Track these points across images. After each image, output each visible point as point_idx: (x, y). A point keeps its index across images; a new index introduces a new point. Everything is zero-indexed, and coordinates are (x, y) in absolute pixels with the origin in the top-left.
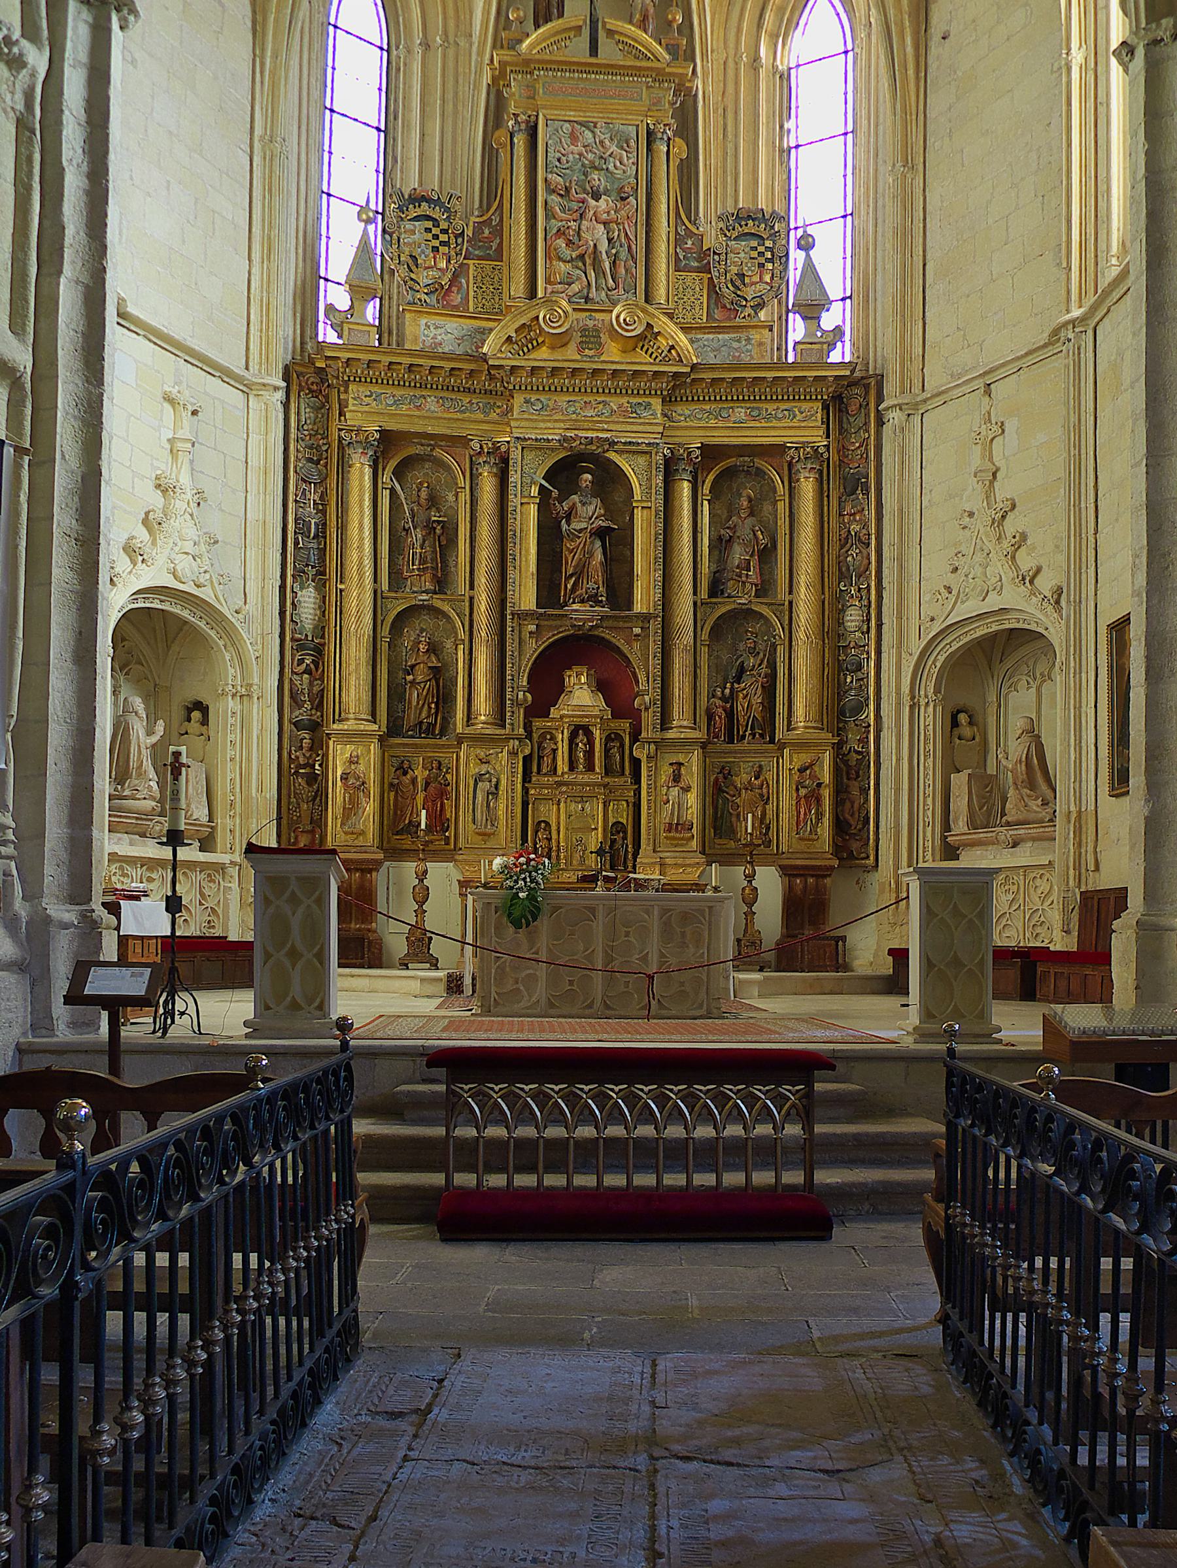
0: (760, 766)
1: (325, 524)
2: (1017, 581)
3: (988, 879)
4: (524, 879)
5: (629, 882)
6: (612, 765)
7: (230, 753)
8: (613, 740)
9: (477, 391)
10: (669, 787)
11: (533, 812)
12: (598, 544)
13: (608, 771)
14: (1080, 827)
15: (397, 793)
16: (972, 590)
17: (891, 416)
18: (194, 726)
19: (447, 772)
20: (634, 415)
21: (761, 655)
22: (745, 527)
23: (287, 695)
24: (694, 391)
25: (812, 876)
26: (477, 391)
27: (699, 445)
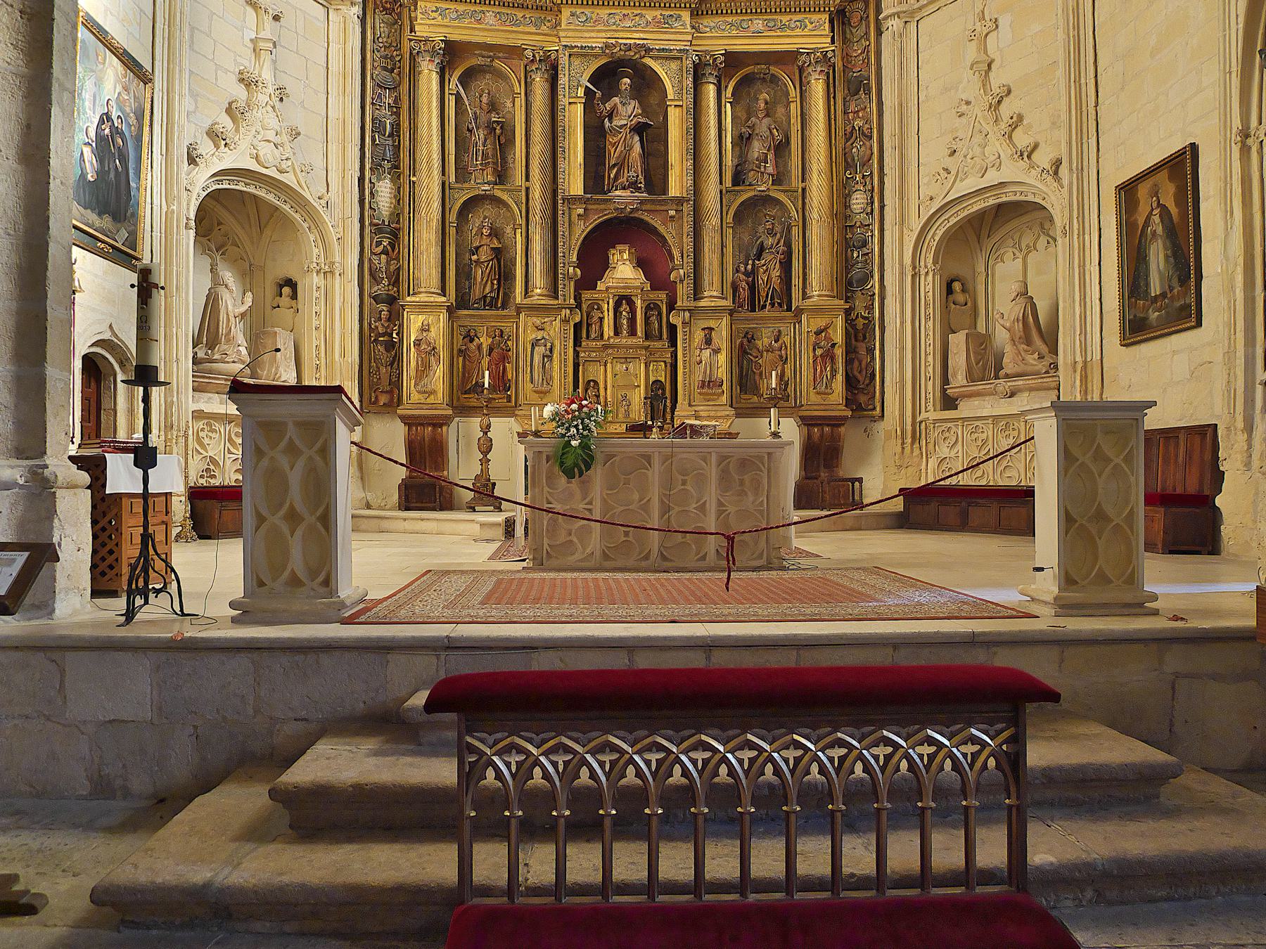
0: (779, 331)
1: (399, 125)
2: (1016, 156)
3: (1137, 415)
4: (576, 427)
5: (685, 427)
6: (651, 331)
7: (315, 323)
8: (652, 309)
9: (530, 7)
10: (701, 349)
11: (584, 373)
12: (637, 138)
13: (648, 336)
14: (1086, 377)
15: (464, 358)
16: (972, 168)
17: (890, 25)
18: (285, 300)
19: (508, 339)
20: (667, 26)
21: (778, 235)
22: (763, 126)
23: (367, 273)
24: (719, 5)
25: (828, 425)
26: (530, 7)
27: (724, 52)
